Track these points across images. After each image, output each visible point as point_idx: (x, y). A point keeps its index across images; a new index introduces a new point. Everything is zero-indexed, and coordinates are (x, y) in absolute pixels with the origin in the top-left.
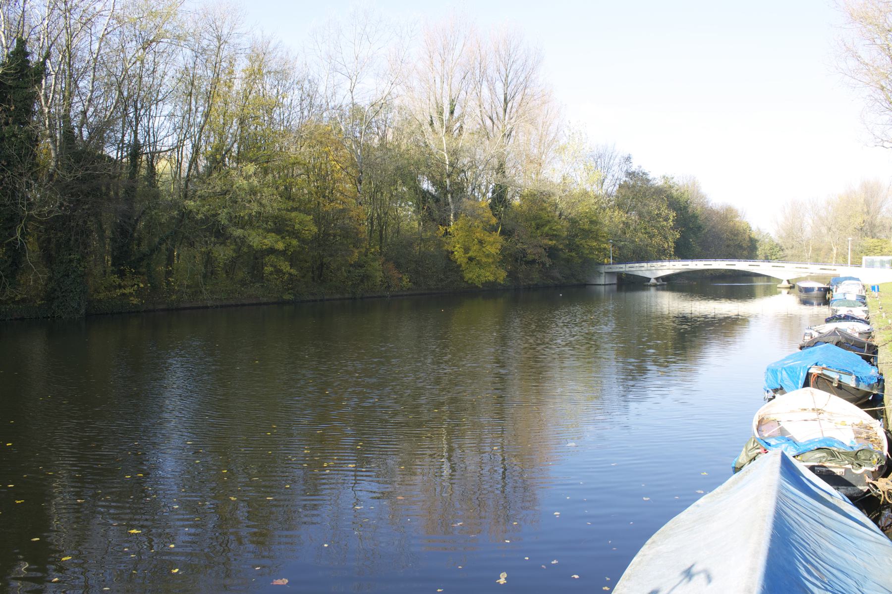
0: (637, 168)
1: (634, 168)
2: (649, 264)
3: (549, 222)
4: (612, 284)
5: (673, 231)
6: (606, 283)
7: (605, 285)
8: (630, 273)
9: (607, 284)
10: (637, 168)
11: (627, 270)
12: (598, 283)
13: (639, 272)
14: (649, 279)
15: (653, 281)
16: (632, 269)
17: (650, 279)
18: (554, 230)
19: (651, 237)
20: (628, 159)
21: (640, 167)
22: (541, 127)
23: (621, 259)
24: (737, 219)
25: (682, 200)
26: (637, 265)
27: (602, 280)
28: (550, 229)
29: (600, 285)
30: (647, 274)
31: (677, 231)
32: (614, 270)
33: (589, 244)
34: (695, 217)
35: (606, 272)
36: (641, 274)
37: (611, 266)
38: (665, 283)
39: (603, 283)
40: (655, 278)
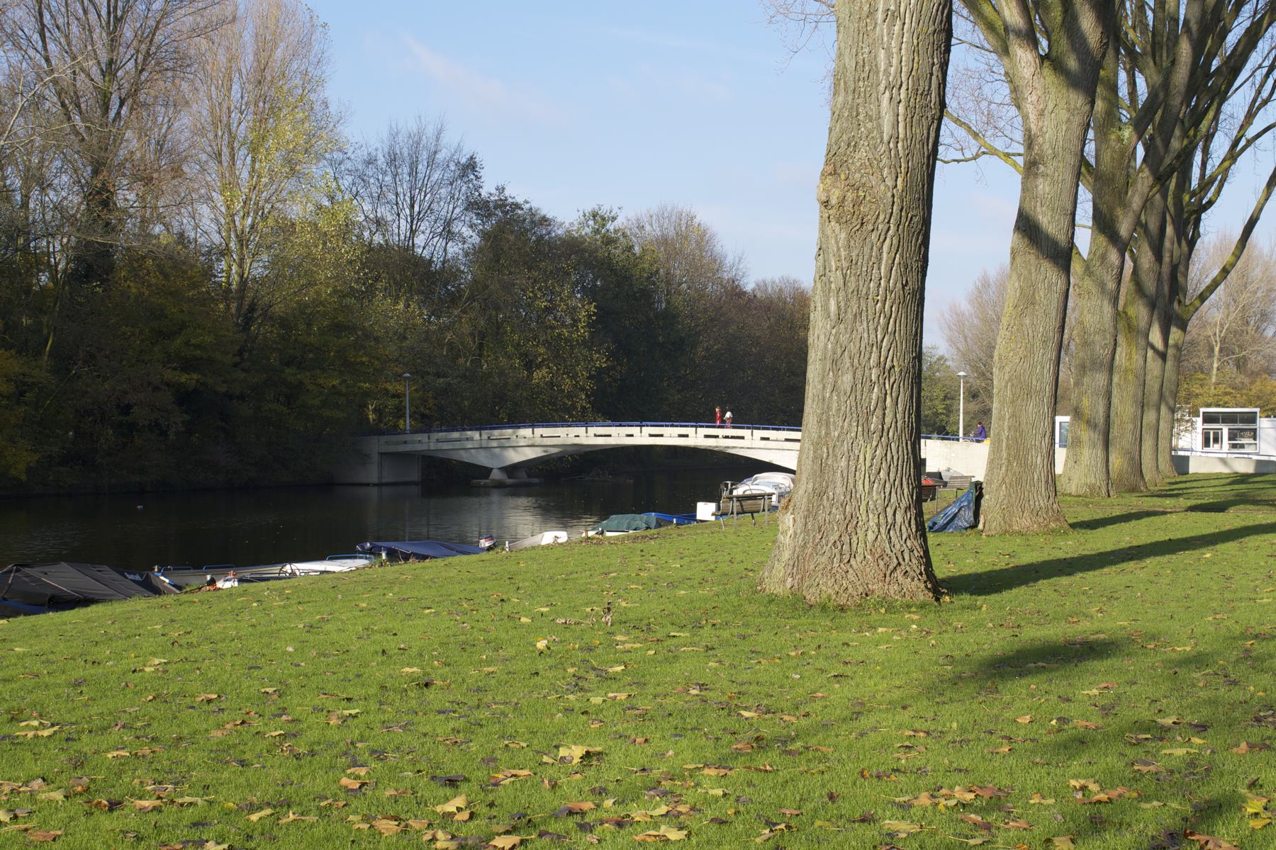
0: (493, 191)
1: (488, 189)
2: (485, 434)
3: (183, 326)
4: (406, 484)
5: (590, 349)
6: (384, 481)
7: (379, 485)
8: (441, 455)
9: (387, 484)
10: (493, 191)
11: (432, 447)
12: (365, 481)
13: (462, 453)
14: (487, 471)
15: (496, 475)
16: (445, 446)
17: (489, 470)
18: (197, 347)
19: (530, 365)
20: (470, 167)
21: (501, 190)
22: (892, 228)
23: (426, 423)
24: (324, 274)
25: (636, 272)
26: (456, 435)
27: (372, 474)
28: (187, 344)
29: (368, 485)
30: (482, 459)
31: (597, 352)
32: (409, 448)
33: (321, 381)
34: (669, 317)
35: (381, 454)
36: (465, 457)
37: (408, 437)
38: (536, 480)
39: (376, 480)
40: (500, 469)
